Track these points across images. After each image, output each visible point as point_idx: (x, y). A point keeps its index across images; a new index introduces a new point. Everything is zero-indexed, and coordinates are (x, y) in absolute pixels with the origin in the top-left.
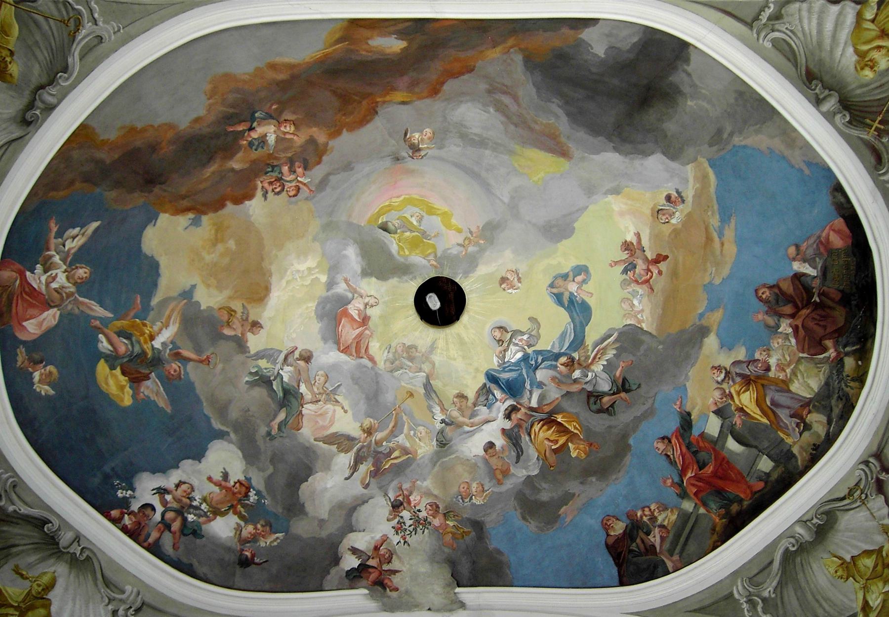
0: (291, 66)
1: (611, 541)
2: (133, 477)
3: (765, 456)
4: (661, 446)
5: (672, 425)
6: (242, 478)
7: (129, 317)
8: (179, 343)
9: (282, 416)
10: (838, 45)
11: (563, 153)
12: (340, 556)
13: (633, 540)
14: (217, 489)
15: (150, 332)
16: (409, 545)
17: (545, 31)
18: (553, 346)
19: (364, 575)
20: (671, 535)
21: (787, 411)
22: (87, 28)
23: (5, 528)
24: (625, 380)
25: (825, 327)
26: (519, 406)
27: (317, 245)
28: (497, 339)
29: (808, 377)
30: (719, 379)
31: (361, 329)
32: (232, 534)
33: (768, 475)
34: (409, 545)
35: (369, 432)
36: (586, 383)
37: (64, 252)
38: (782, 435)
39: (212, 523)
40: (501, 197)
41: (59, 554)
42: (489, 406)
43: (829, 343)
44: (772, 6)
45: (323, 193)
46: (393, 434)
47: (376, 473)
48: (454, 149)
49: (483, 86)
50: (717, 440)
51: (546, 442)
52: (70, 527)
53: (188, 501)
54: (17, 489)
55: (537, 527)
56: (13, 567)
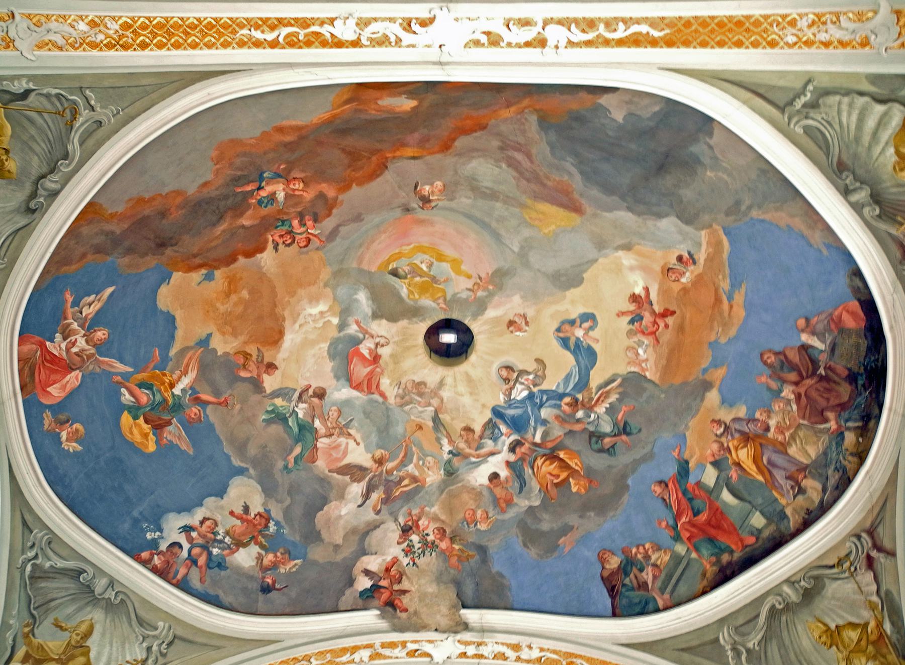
0: (299, 128)
1: (606, 574)
2: (159, 519)
3: (758, 513)
4: (658, 490)
5: (670, 471)
6: (262, 510)
7: (149, 369)
8: (198, 388)
9: (298, 450)
10: (877, 143)
11: (577, 209)
12: (354, 577)
13: (627, 574)
14: (238, 522)
15: (170, 380)
16: (417, 566)
17: (562, 94)
18: (558, 386)
19: (376, 595)
20: (663, 575)
21: (783, 473)
22: (84, 115)
23: (43, 585)
24: (626, 424)
25: (828, 400)
26: (523, 441)
27: (328, 290)
28: (504, 377)
29: (806, 443)
30: (719, 433)
31: (372, 367)
32: (254, 563)
33: (760, 531)
34: (417, 566)
35: (380, 462)
36: (589, 423)
37: (81, 319)
38: (775, 494)
39: (236, 555)
40: (510, 246)
41: (95, 601)
42: (495, 440)
43: (831, 415)
44: (809, 95)
45: (334, 243)
46: (403, 464)
47: (386, 501)
48: (464, 200)
49: (496, 143)
50: (712, 491)
51: (549, 477)
52: (103, 573)
53: (212, 536)
54: (52, 545)
55: (538, 555)
56: (52, 621)
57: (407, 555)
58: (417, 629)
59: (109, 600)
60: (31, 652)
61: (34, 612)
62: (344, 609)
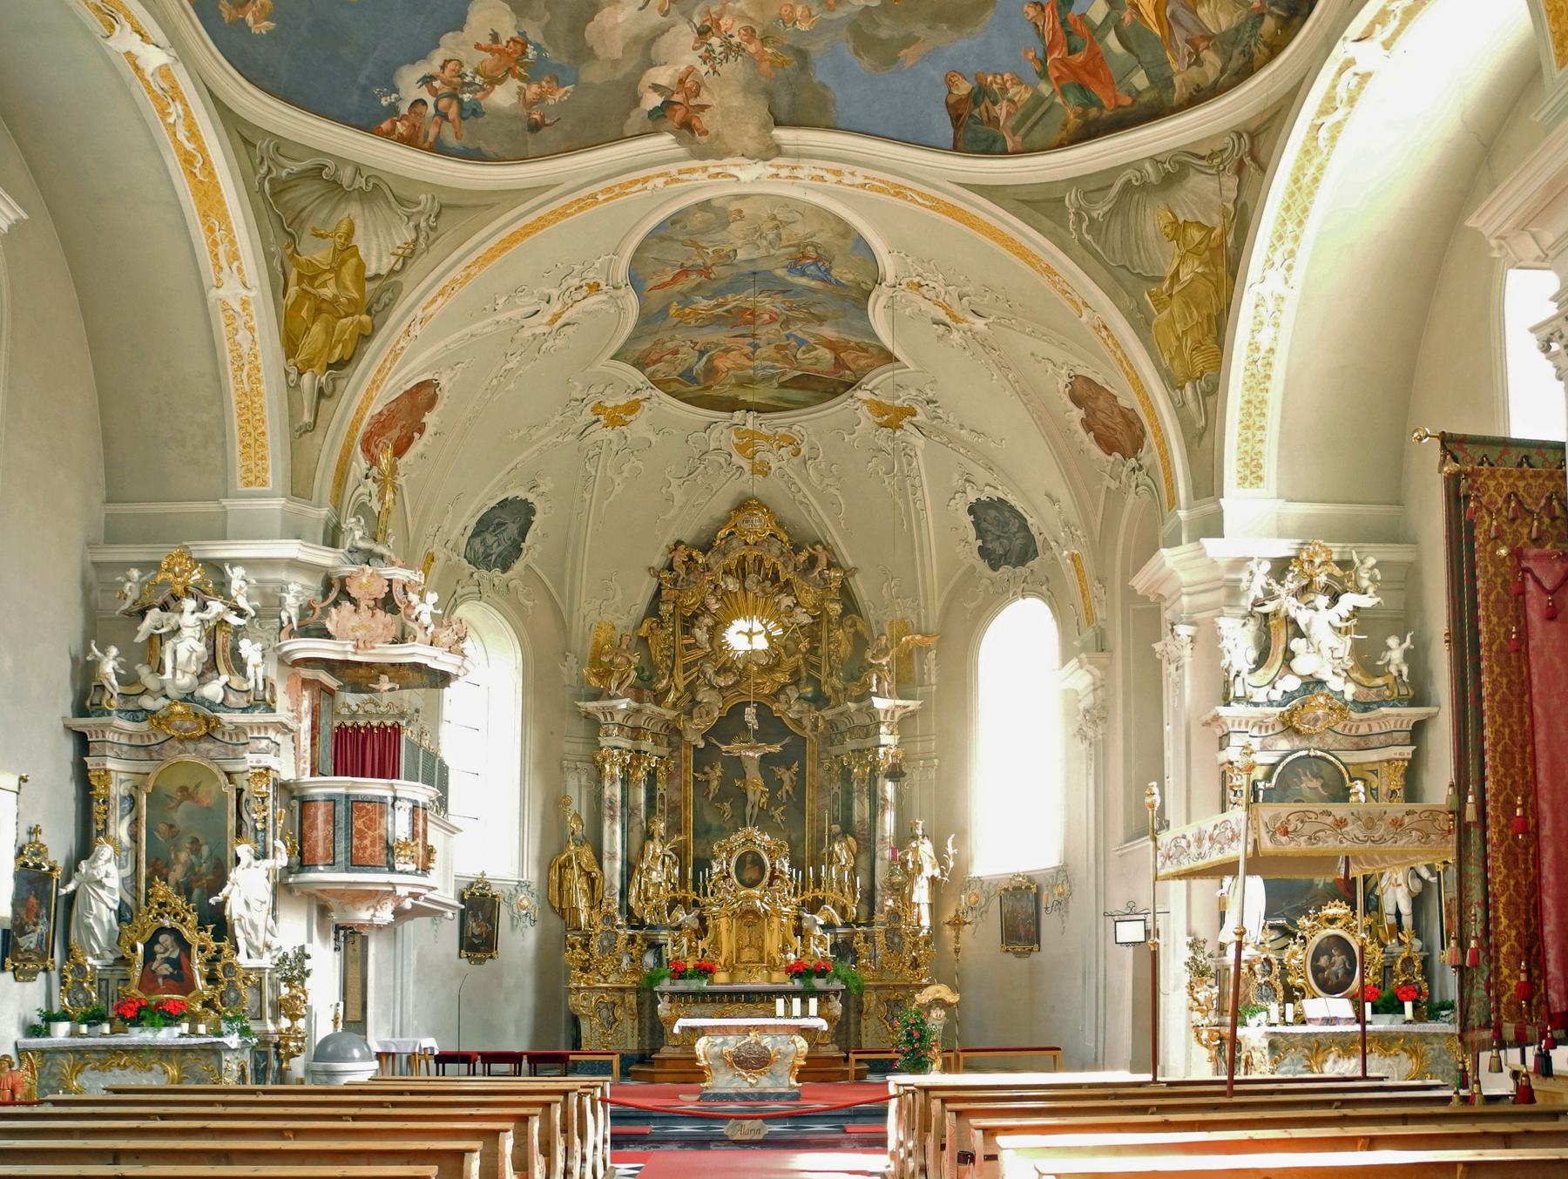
1: (952, 100)
2: (392, 77)
3: (1143, 71)
4: (1032, 12)
6: (515, 35)
13: (977, 105)
14: (488, 55)
20: (1018, 115)
21: (1184, 34)
33: (1139, 93)
39: (492, 95)
52: (345, 161)
54: (281, 150)
56: (310, 231)
57: (705, 63)
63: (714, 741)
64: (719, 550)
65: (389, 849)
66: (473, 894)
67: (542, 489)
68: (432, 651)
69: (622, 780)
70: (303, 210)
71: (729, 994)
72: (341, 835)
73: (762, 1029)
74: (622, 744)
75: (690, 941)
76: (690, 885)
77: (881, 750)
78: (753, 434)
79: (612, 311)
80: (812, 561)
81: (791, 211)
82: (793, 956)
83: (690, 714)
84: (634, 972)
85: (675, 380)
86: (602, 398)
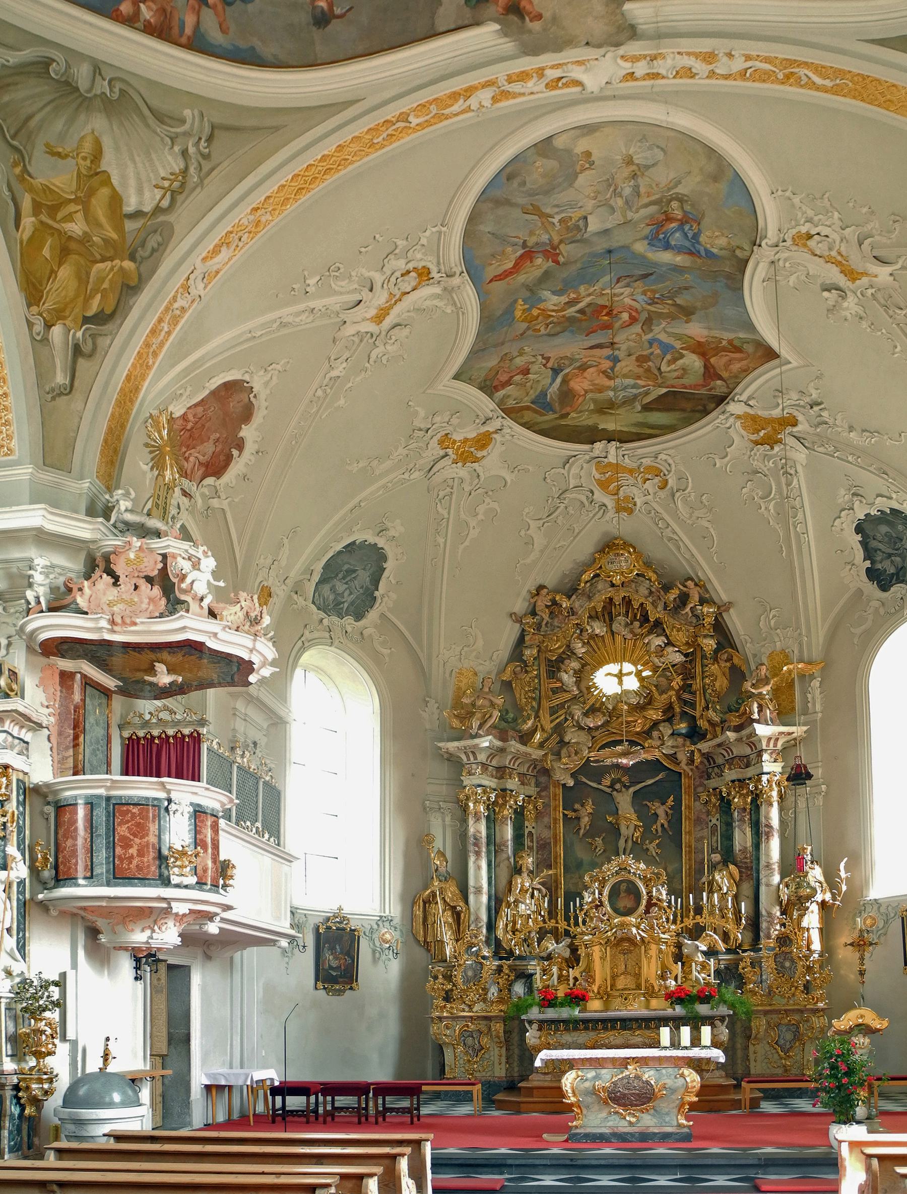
23: (6, 98)
52: (81, 57)
58: (558, 46)
59: (103, 96)
60: (38, 199)
61: (15, 143)
62: (445, 29)
63: (584, 780)
64: (583, 594)
65: (161, 858)
66: (329, 928)
67: (392, 533)
68: (212, 626)
69: (488, 818)
70: (30, 118)
71: (604, 1021)
72: (101, 844)
73: (643, 1062)
74: (486, 783)
75: (560, 969)
76: (561, 916)
77: (765, 778)
78: (617, 468)
79: (449, 311)
80: (684, 599)
81: (650, 148)
82: (673, 983)
83: (558, 754)
84: (501, 1001)
85: (528, 408)
86: (449, 429)
